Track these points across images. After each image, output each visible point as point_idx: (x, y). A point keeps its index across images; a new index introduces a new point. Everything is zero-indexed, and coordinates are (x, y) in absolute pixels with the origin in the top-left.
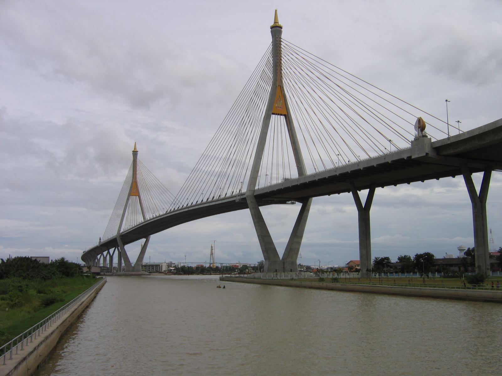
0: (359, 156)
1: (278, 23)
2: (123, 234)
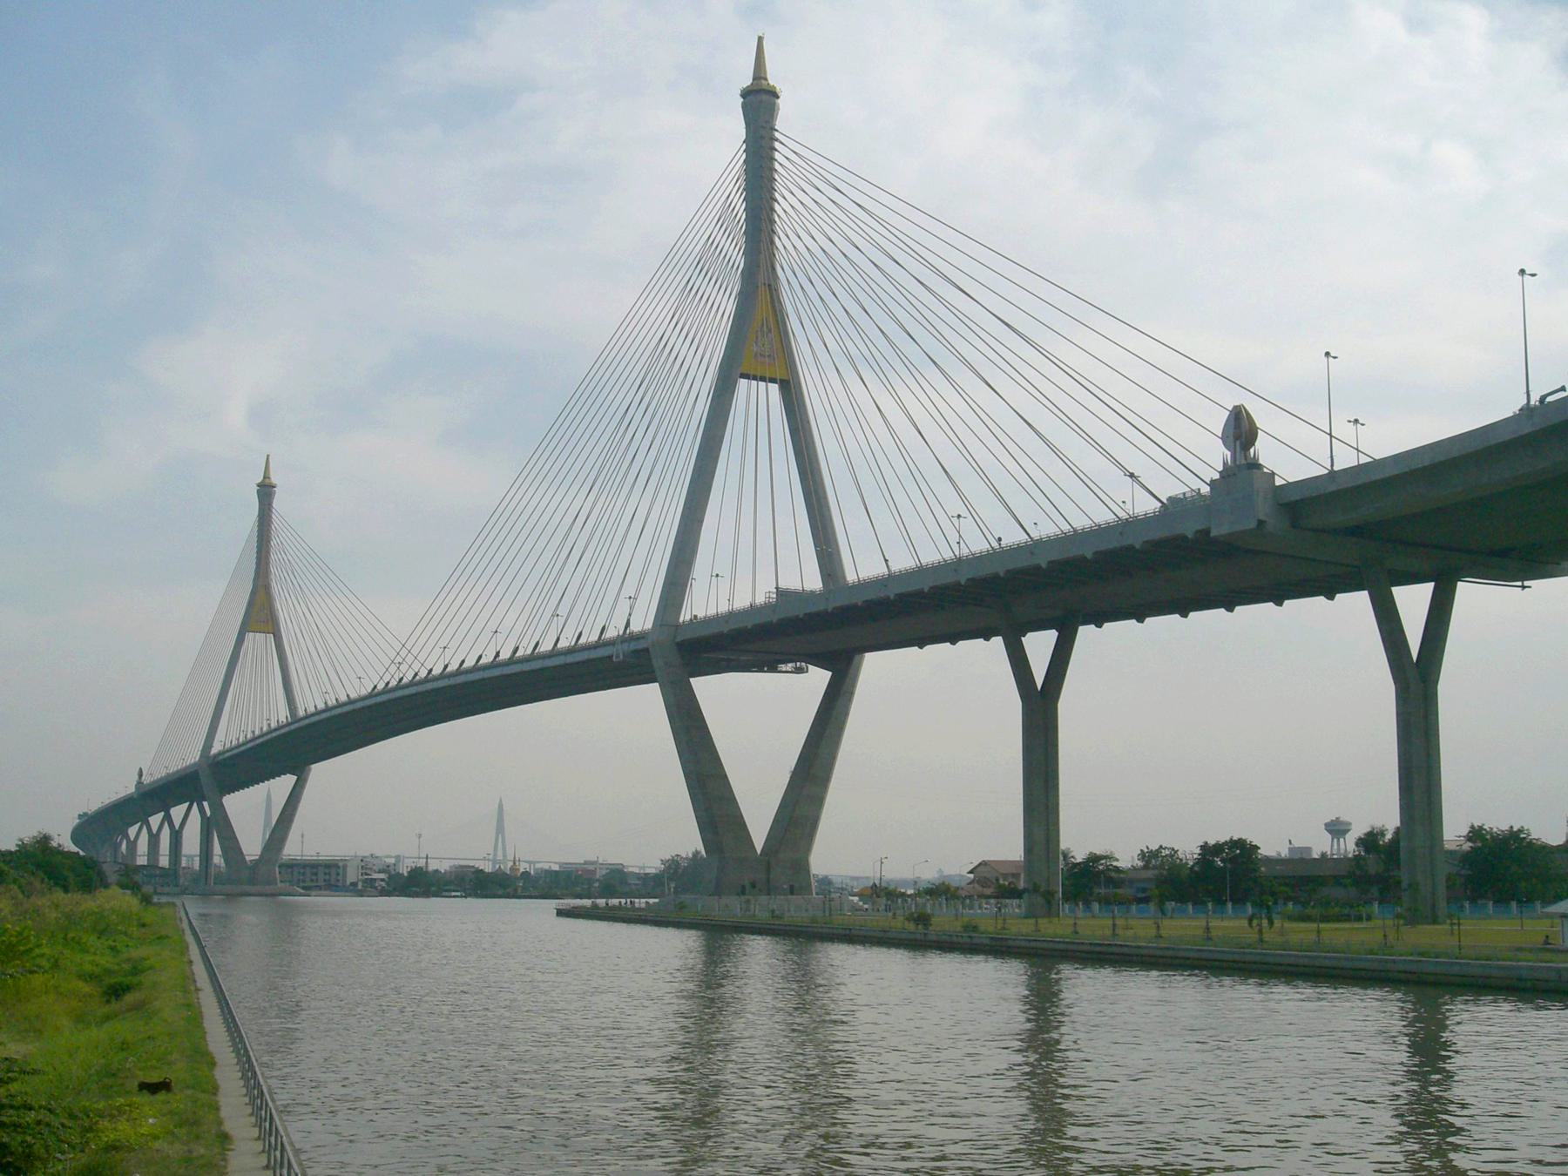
0: (1124, 502)
1: (766, 79)
2: (221, 757)
